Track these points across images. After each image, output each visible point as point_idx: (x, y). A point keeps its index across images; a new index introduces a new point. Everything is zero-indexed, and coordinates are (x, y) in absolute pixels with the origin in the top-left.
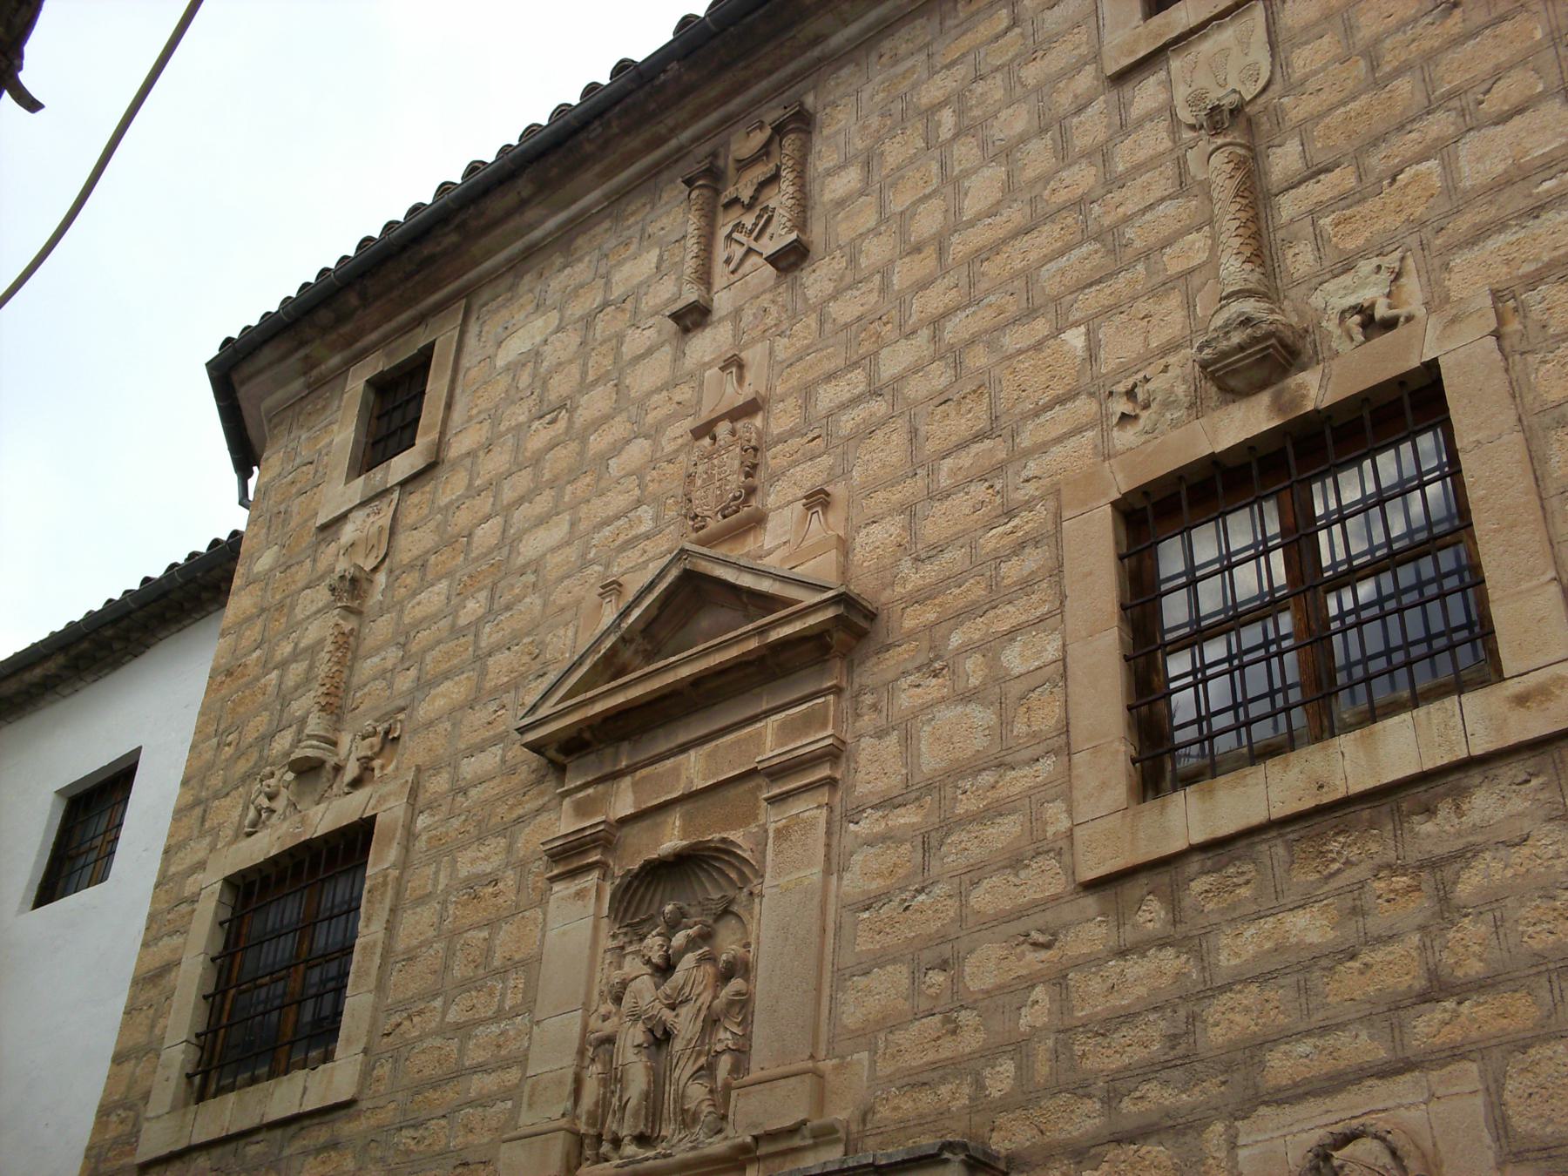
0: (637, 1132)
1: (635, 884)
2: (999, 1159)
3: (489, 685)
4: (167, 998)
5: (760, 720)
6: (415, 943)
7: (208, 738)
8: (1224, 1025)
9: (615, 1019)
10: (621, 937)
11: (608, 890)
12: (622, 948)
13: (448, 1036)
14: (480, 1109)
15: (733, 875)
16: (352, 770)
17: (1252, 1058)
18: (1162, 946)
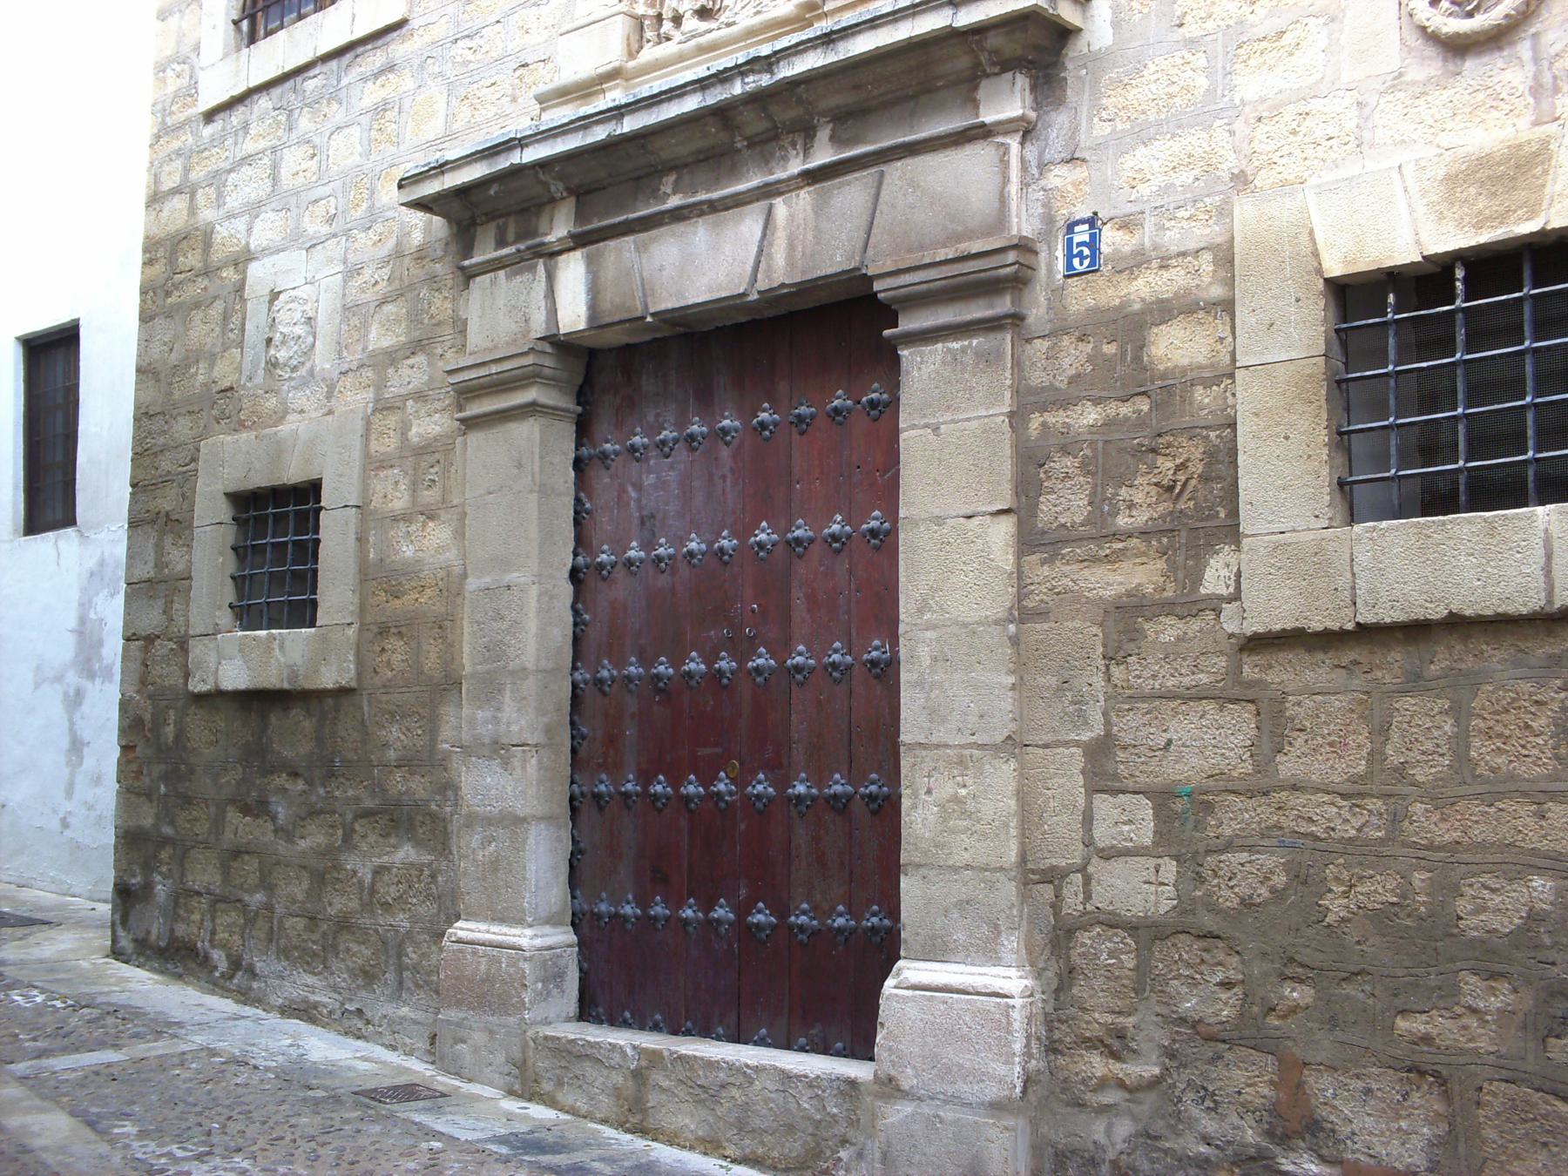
0: (697, 6)
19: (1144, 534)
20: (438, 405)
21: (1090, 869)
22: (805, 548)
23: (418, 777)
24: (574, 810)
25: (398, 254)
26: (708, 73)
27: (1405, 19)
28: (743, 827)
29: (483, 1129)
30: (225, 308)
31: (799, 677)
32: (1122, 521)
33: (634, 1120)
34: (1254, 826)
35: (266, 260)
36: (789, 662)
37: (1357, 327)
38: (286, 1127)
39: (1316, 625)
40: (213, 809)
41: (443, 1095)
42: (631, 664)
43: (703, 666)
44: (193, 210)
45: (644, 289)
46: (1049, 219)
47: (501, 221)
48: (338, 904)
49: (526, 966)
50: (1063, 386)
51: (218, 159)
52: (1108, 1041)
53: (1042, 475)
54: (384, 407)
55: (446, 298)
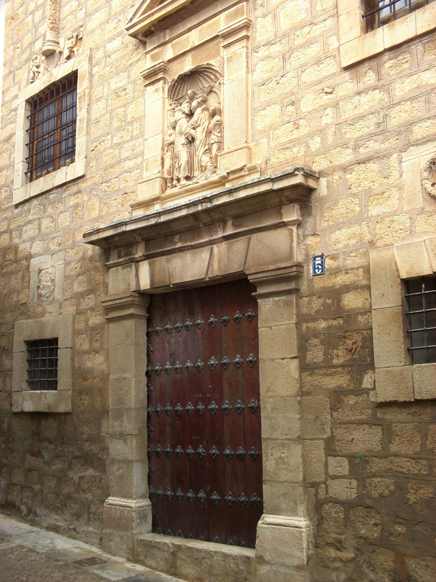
0: (185, 176)
1: (176, 84)
2: (316, 173)
3: (113, 13)
4: (13, 147)
5: (218, 15)
6: (98, 116)
7: (10, 46)
8: (397, 118)
9: (173, 136)
10: (173, 105)
11: (167, 87)
12: (174, 109)
13: (114, 148)
14: (129, 173)
15: (213, 77)
16: (66, 53)
17: (408, 129)
18: (374, 90)
19: (342, 366)
20: (98, 313)
21: (328, 483)
22: (227, 366)
23: (94, 445)
24: (149, 457)
25: (83, 258)
26: (189, 202)
27: (424, 190)
28: (208, 465)
29: (119, 576)
30: (23, 274)
31: (226, 412)
32: (335, 361)
33: (172, 570)
34: (383, 469)
35: (37, 258)
36: (223, 406)
37: (412, 295)
38: (49, 578)
39: (401, 399)
40: (21, 454)
41: (105, 562)
42: (168, 406)
43: (193, 407)
44: (11, 239)
45: (169, 275)
46: (307, 255)
47: (119, 249)
48: (67, 489)
49: (133, 514)
50: (313, 314)
51: (20, 221)
52: (336, 544)
53: (307, 345)
54: (79, 312)
55: (100, 275)
